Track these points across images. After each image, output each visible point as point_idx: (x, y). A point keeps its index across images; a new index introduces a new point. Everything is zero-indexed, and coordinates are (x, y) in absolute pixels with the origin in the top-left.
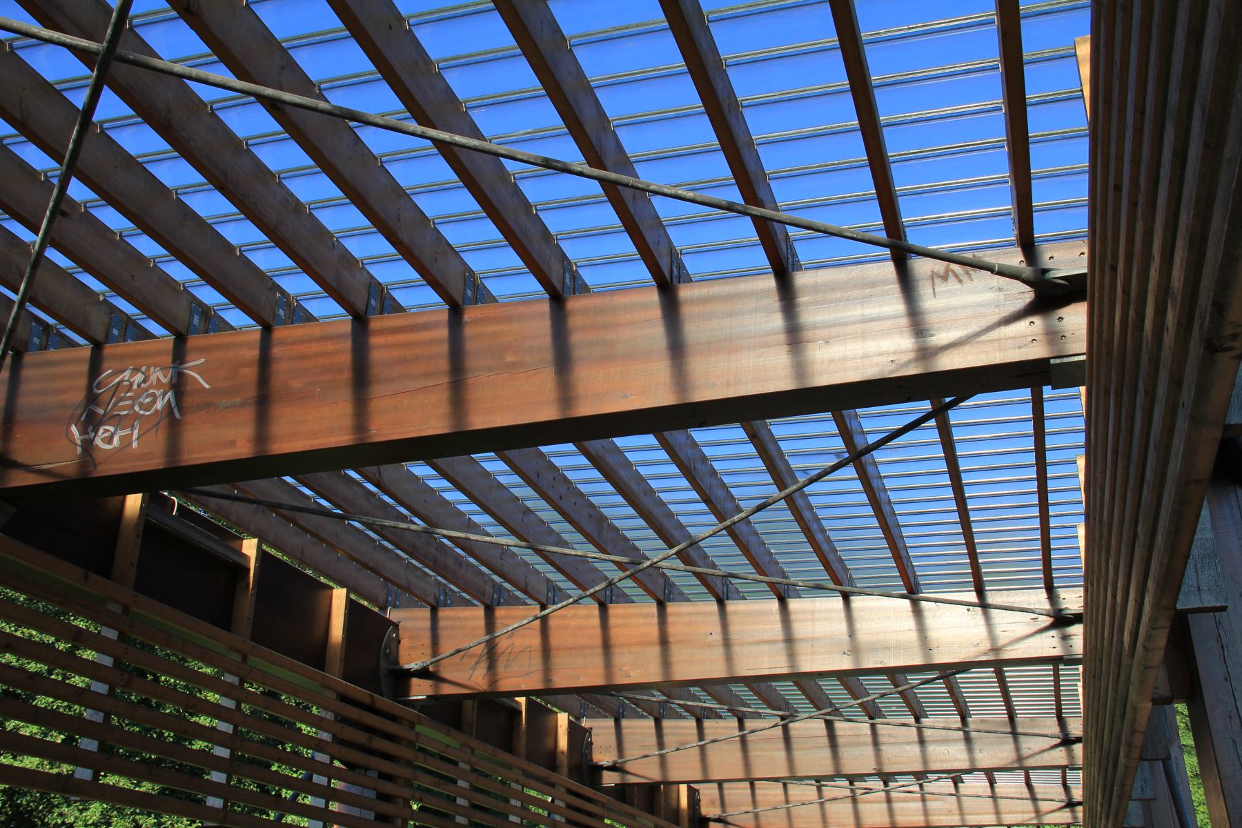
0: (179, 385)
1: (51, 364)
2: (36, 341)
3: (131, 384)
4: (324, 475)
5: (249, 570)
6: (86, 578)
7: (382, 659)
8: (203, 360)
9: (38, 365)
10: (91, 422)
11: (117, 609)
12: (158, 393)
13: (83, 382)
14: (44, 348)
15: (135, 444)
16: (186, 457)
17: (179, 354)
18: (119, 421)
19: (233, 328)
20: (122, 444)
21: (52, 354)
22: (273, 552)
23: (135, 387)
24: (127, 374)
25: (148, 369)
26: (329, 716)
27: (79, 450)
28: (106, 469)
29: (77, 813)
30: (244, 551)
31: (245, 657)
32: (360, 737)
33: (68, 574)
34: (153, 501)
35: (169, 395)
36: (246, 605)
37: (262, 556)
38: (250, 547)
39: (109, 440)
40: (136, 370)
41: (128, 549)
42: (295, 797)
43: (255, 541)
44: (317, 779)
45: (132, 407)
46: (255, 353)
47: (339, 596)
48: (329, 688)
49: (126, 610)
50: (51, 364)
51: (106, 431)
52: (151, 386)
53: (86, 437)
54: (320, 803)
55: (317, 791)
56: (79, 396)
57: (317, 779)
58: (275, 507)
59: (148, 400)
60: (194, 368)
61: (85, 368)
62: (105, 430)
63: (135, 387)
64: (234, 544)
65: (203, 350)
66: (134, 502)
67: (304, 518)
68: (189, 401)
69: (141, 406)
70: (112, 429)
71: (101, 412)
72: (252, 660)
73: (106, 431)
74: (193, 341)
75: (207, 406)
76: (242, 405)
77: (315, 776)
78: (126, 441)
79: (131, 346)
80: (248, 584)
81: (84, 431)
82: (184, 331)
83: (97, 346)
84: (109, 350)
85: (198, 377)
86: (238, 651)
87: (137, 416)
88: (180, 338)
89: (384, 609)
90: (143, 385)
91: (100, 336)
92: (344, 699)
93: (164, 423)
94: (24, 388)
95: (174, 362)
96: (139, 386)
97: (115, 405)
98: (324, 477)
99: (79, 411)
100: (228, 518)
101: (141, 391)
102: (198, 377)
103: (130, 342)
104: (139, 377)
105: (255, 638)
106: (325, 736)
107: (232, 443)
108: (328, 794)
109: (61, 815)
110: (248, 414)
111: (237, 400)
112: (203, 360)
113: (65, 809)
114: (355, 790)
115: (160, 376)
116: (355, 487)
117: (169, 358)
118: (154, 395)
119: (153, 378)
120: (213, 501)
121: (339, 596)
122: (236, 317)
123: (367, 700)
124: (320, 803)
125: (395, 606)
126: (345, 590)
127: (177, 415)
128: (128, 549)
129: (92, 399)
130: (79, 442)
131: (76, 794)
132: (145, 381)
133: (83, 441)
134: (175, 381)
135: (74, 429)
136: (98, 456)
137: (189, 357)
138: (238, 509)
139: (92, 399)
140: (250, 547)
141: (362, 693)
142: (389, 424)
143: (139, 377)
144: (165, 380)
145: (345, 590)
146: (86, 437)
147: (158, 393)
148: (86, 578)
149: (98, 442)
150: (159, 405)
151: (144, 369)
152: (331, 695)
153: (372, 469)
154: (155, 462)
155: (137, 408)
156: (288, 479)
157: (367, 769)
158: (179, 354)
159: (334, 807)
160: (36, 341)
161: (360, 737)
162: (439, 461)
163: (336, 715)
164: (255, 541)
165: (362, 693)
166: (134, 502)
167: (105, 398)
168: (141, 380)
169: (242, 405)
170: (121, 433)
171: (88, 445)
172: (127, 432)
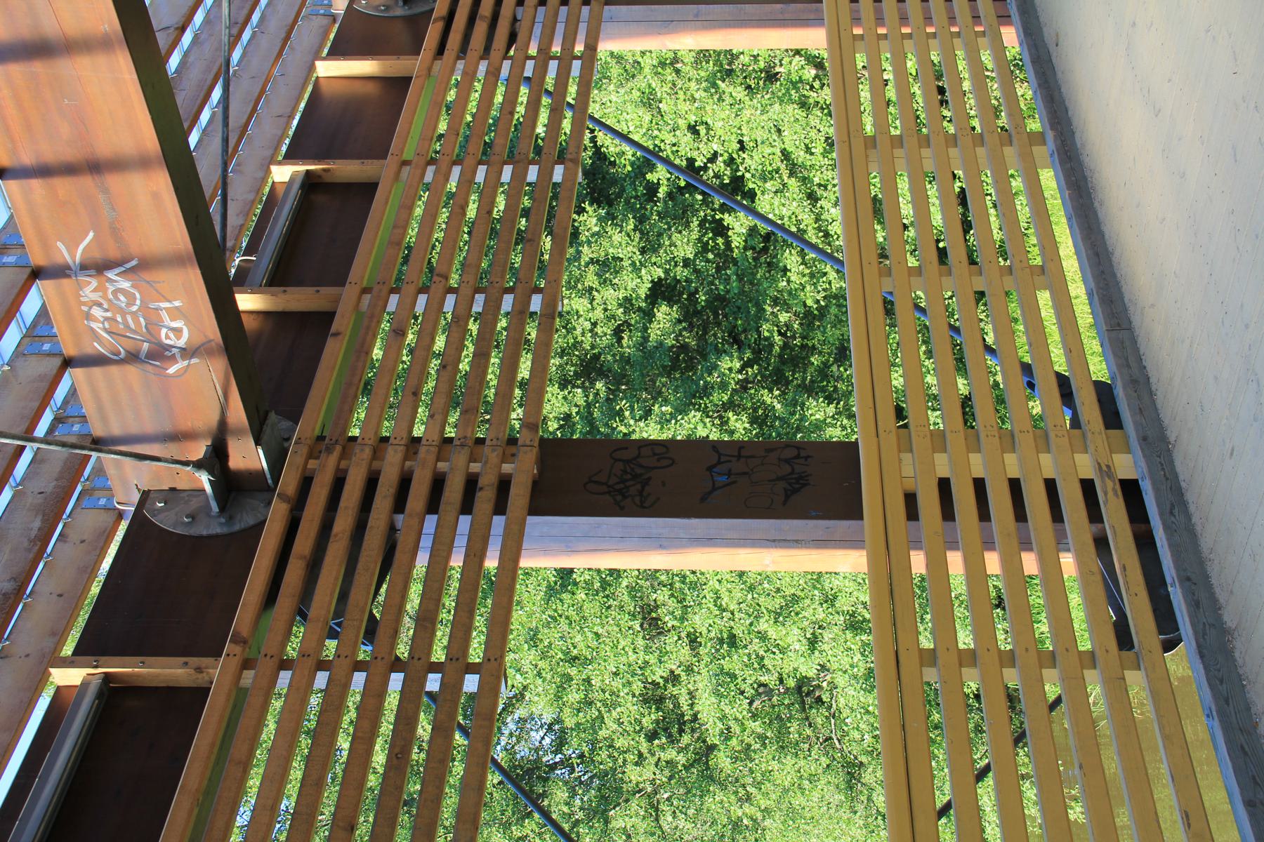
0: (98, 267)
1: (100, 409)
2: (76, 428)
3: (107, 319)
4: (181, 99)
5: (308, 172)
6: (336, 334)
7: (391, 14)
8: (59, 244)
9: (104, 420)
10: (160, 354)
11: (367, 298)
12: (111, 288)
13: (114, 370)
14: (83, 419)
15: (177, 303)
16: (181, 246)
17: (60, 272)
18: (153, 324)
19: (11, 217)
20: (179, 312)
21: (89, 408)
22: (284, 148)
23: (109, 314)
24: (95, 326)
25: (84, 304)
26: (460, 65)
27: (194, 361)
28: (211, 330)
29: (581, 320)
30: (286, 179)
31: (405, 163)
32: (481, 28)
33: (334, 352)
34: (243, 280)
35: (111, 275)
36: (346, 169)
37: (291, 156)
38: (282, 174)
39: (178, 332)
40: (88, 316)
41: (298, 299)
42: (548, 93)
43: (274, 168)
44: (528, 72)
45: (134, 314)
46: (36, 183)
47: (327, 69)
48: (430, 69)
49: (366, 291)
50: (100, 409)
51: (167, 337)
52: (105, 297)
53: (178, 356)
54: (553, 65)
55: (542, 69)
56: (132, 371)
57: (528, 72)
58: (227, 155)
59: (122, 298)
60: (70, 253)
61: (97, 371)
62: (166, 337)
63: (109, 314)
64: (280, 191)
65: (46, 246)
66: (247, 302)
67: (235, 120)
68: (113, 253)
69: (130, 304)
70: (164, 331)
71: (146, 345)
72: (408, 154)
73: (167, 337)
74: (38, 258)
75: (115, 232)
76: (106, 191)
77: (525, 75)
78: (175, 313)
79: (60, 326)
80: (324, 170)
81: (173, 359)
82: (28, 271)
83: (68, 363)
84: (70, 350)
85: (82, 247)
86: (399, 171)
87: (144, 307)
88: (37, 274)
89: (334, 18)
90: (106, 306)
91: (57, 362)
92: (441, 50)
93: (146, 276)
94: (134, 428)
95: (69, 276)
96: (107, 310)
97: (135, 332)
98: (183, 99)
99: (150, 368)
100: (253, 202)
101: (112, 307)
102: (82, 247)
103: (55, 330)
104: (97, 312)
105: (383, 155)
106: (483, 67)
107: (156, 196)
108: (545, 56)
109: (583, 334)
110: (114, 181)
111: (101, 197)
112: (59, 244)
113: (578, 332)
114: (537, 30)
115: (89, 288)
116: (191, 59)
117: (65, 281)
118: (115, 292)
119: (95, 296)
120: (233, 220)
121: (327, 69)
122: (30, 306)
123: (440, 26)
124: (553, 65)
125: (330, 6)
126: (318, 63)
127: (134, 263)
128: (298, 299)
129: (133, 357)
130: (186, 363)
131: (555, 306)
132: (100, 305)
133: (184, 357)
134: (93, 272)
135: (171, 371)
136: (198, 340)
137: (59, 260)
138: (239, 191)
139: (133, 357)
140: (282, 174)
141: (433, 33)
142: (133, 127)
143: (97, 312)
144: (94, 283)
145: (318, 63)
146: (178, 356)
147: (111, 288)
148: (336, 334)
149: (182, 343)
150: (125, 285)
151: (85, 308)
152: (438, 64)
153: (162, 40)
154: (194, 278)
155: (135, 308)
156: (193, 139)
157: (515, 20)
158: (60, 272)
159: (556, 49)
160: (76, 428)
161: (481, 28)
162: (186, 125)
163: (458, 58)
164: (274, 168)
165: (433, 33)
166: (247, 302)
167: (130, 345)
168: (98, 311)
169: (106, 191)
170: (167, 321)
171: (186, 353)
172: (164, 315)
